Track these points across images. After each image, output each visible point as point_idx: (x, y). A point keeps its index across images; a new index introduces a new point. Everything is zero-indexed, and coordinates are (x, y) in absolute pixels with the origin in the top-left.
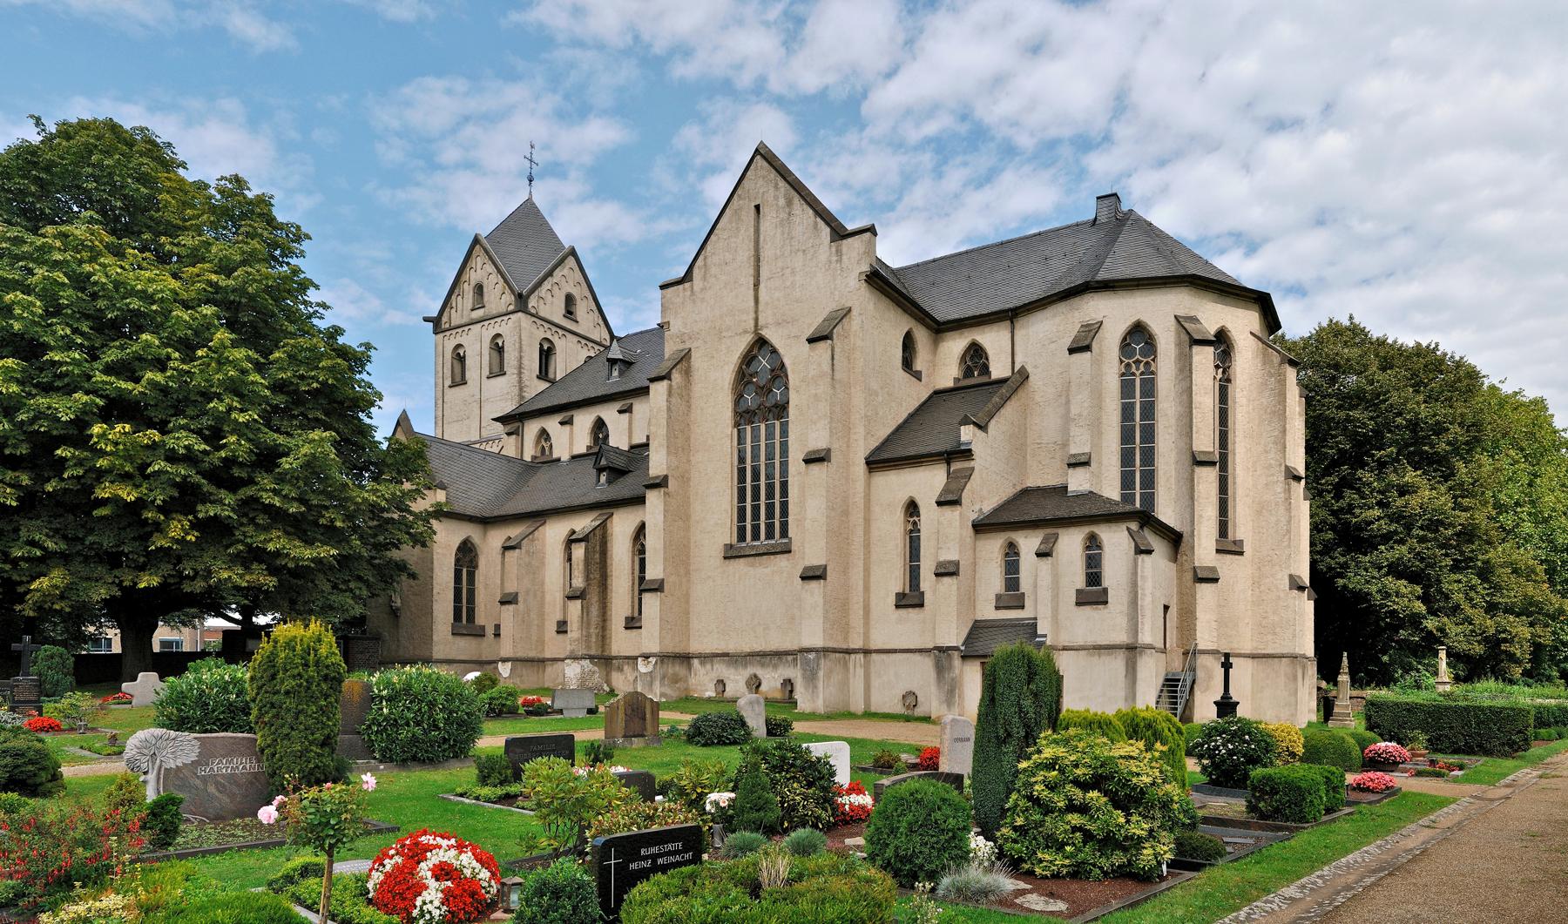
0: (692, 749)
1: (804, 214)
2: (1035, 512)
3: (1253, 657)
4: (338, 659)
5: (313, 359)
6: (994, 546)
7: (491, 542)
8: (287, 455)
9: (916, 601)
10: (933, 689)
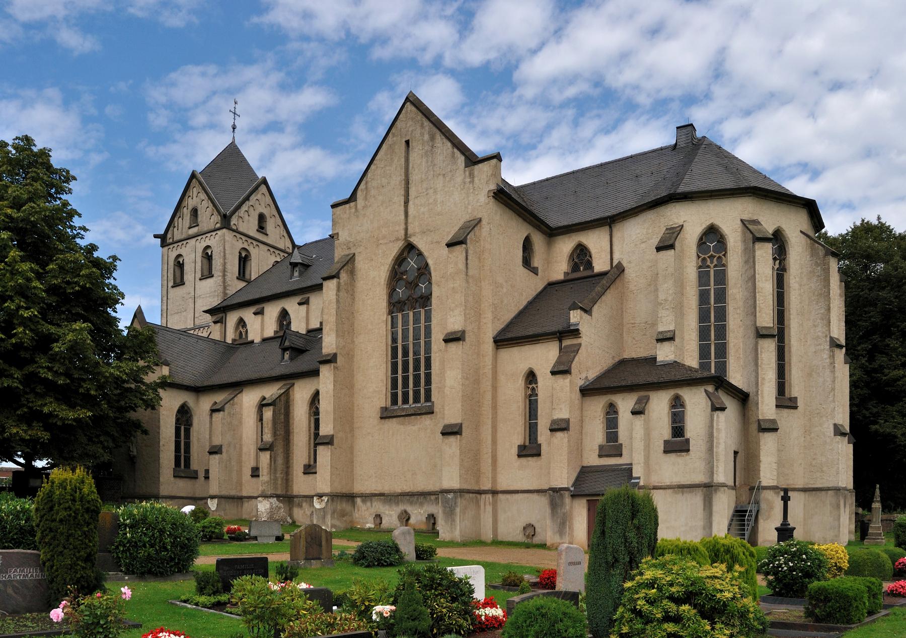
0: (357, 570)
1: (444, 147)
2: (632, 378)
3: (805, 490)
4: (95, 496)
5: (77, 268)
6: (597, 406)
7: (202, 406)
8: (57, 341)
9: (534, 452)
10: (548, 522)
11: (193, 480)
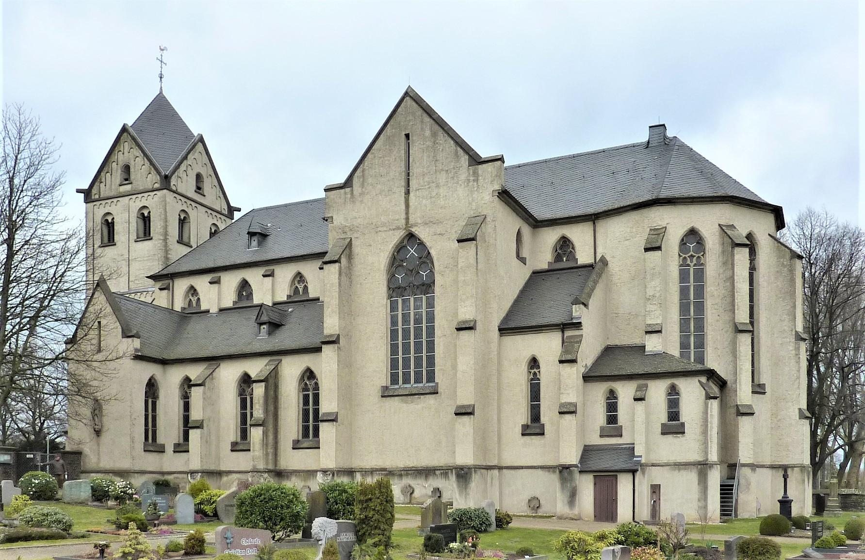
2: (616, 366)
6: (599, 391)
9: (538, 431)
11: (161, 454)
